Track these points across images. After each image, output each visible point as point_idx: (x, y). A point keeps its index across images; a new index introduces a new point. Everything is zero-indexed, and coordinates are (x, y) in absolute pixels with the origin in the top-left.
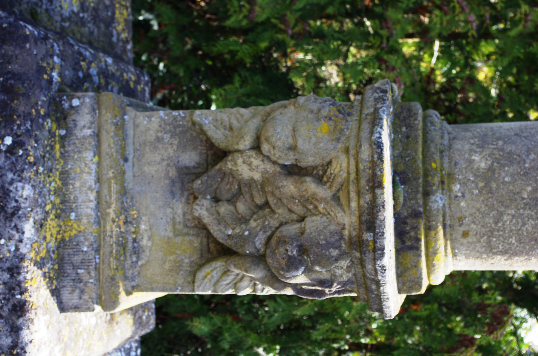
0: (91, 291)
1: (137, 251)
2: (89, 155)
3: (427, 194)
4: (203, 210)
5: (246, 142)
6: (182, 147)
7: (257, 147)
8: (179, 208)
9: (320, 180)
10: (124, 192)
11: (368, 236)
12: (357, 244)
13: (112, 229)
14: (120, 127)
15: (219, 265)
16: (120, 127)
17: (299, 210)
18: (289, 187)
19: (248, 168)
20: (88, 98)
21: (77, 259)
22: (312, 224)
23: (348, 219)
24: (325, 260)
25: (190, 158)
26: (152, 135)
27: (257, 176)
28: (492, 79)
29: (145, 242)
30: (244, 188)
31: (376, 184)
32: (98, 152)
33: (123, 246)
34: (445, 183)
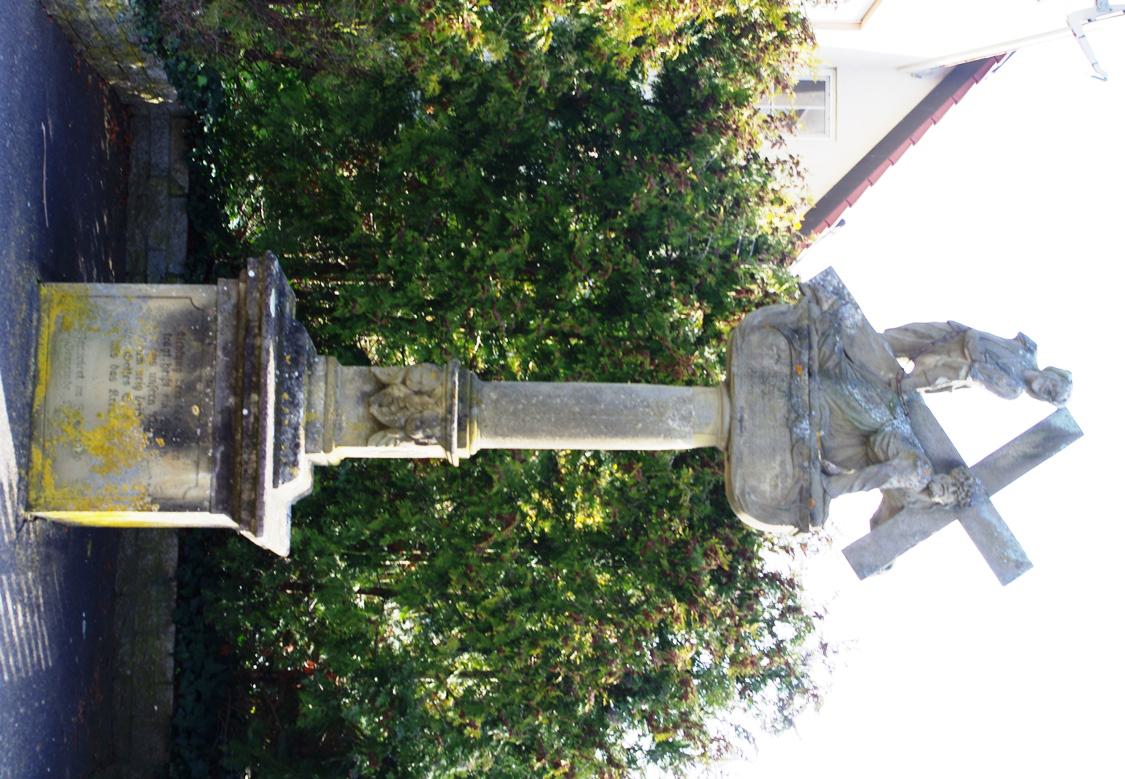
0: (320, 444)
1: (340, 429)
2: (322, 384)
3: (471, 408)
4: (374, 410)
5: (400, 379)
6: (364, 383)
7: (404, 382)
8: (361, 410)
9: (429, 396)
10: (336, 402)
11: (449, 416)
12: (445, 420)
13: (331, 417)
14: (336, 371)
15: (381, 433)
16: (336, 371)
17: (420, 408)
18: (417, 399)
19: (398, 391)
20: (323, 358)
21: (314, 430)
22: (426, 413)
23: (441, 411)
24: (431, 427)
25: (368, 388)
26: (350, 377)
27: (402, 395)
28: (649, 718)
29: (344, 425)
30: (394, 400)
31: (453, 396)
32: (326, 383)
33: (335, 425)
34: (479, 404)
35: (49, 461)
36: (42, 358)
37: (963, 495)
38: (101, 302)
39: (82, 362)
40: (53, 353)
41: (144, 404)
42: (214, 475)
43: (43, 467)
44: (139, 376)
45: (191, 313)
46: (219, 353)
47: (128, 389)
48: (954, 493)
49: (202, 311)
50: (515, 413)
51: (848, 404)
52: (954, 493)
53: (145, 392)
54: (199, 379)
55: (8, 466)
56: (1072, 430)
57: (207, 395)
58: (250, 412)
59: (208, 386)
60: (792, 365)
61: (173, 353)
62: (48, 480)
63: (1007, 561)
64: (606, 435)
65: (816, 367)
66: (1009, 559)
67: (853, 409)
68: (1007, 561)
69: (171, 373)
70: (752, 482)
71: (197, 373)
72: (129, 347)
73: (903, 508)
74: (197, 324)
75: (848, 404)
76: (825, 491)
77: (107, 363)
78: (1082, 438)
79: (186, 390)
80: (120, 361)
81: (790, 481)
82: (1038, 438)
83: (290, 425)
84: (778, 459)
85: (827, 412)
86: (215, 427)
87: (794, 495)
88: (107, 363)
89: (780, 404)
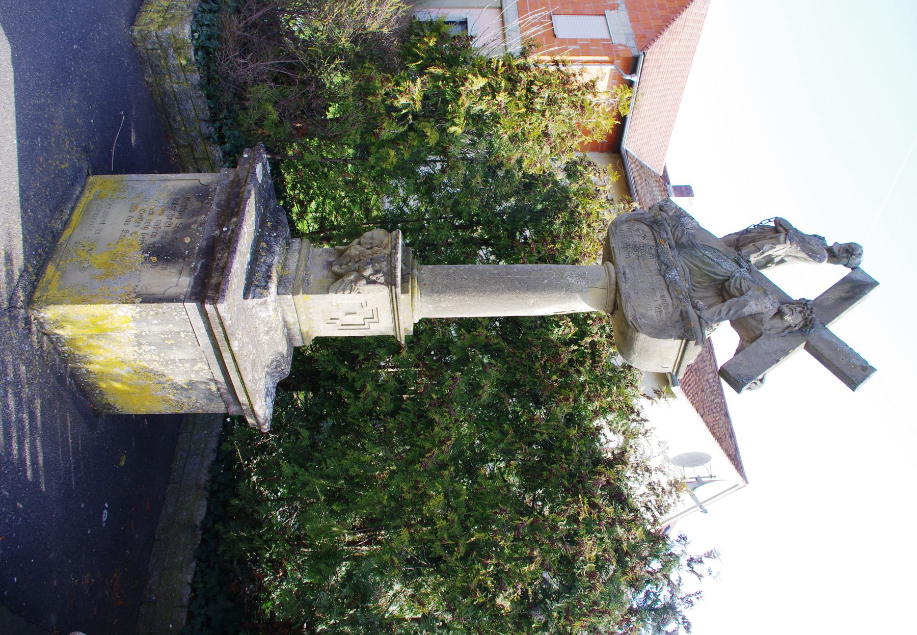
1: (308, 283)
2: (296, 254)
3: (412, 269)
10: (306, 266)
12: (390, 255)
13: (301, 273)
24: (379, 261)
35: (60, 273)
36: (77, 213)
37: (808, 312)
38: (131, 183)
39: (106, 214)
40: (87, 210)
41: (147, 237)
42: (195, 278)
43: (53, 276)
44: (149, 221)
45: (197, 187)
46: (214, 207)
47: (137, 229)
48: (801, 312)
49: (207, 186)
50: (447, 275)
51: (703, 262)
52: (801, 312)
53: (150, 230)
54: (195, 222)
55: (9, 258)
56: (869, 281)
57: (199, 231)
58: (228, 230)
59: (201, 226)
60: (655, 239)
61: (178, 208)
62: (54, 284)
63: (851, 370)
64: (519, 289)
65: (673, 243)
66: (856, 366)
67: (708, 264)
68: (851, 370)
69: (174, 219)
70: (641, 310)
71: (195, 218)
72: (145, 206)
73: (761, 335)
74: (203, 193)
75: (703, 262)
76: (699, 317)
77: (126, 214)
78: (877, 288)
79: (185, 228)
80: (136, 214)
81: (671, 309)
82: (847, 287)
83: (265, 262)
84: (658, 294)
85: (687, 270)
86: (201, 249)
87: (677, 317)
88: (126, 214)
89: (653, 264)
